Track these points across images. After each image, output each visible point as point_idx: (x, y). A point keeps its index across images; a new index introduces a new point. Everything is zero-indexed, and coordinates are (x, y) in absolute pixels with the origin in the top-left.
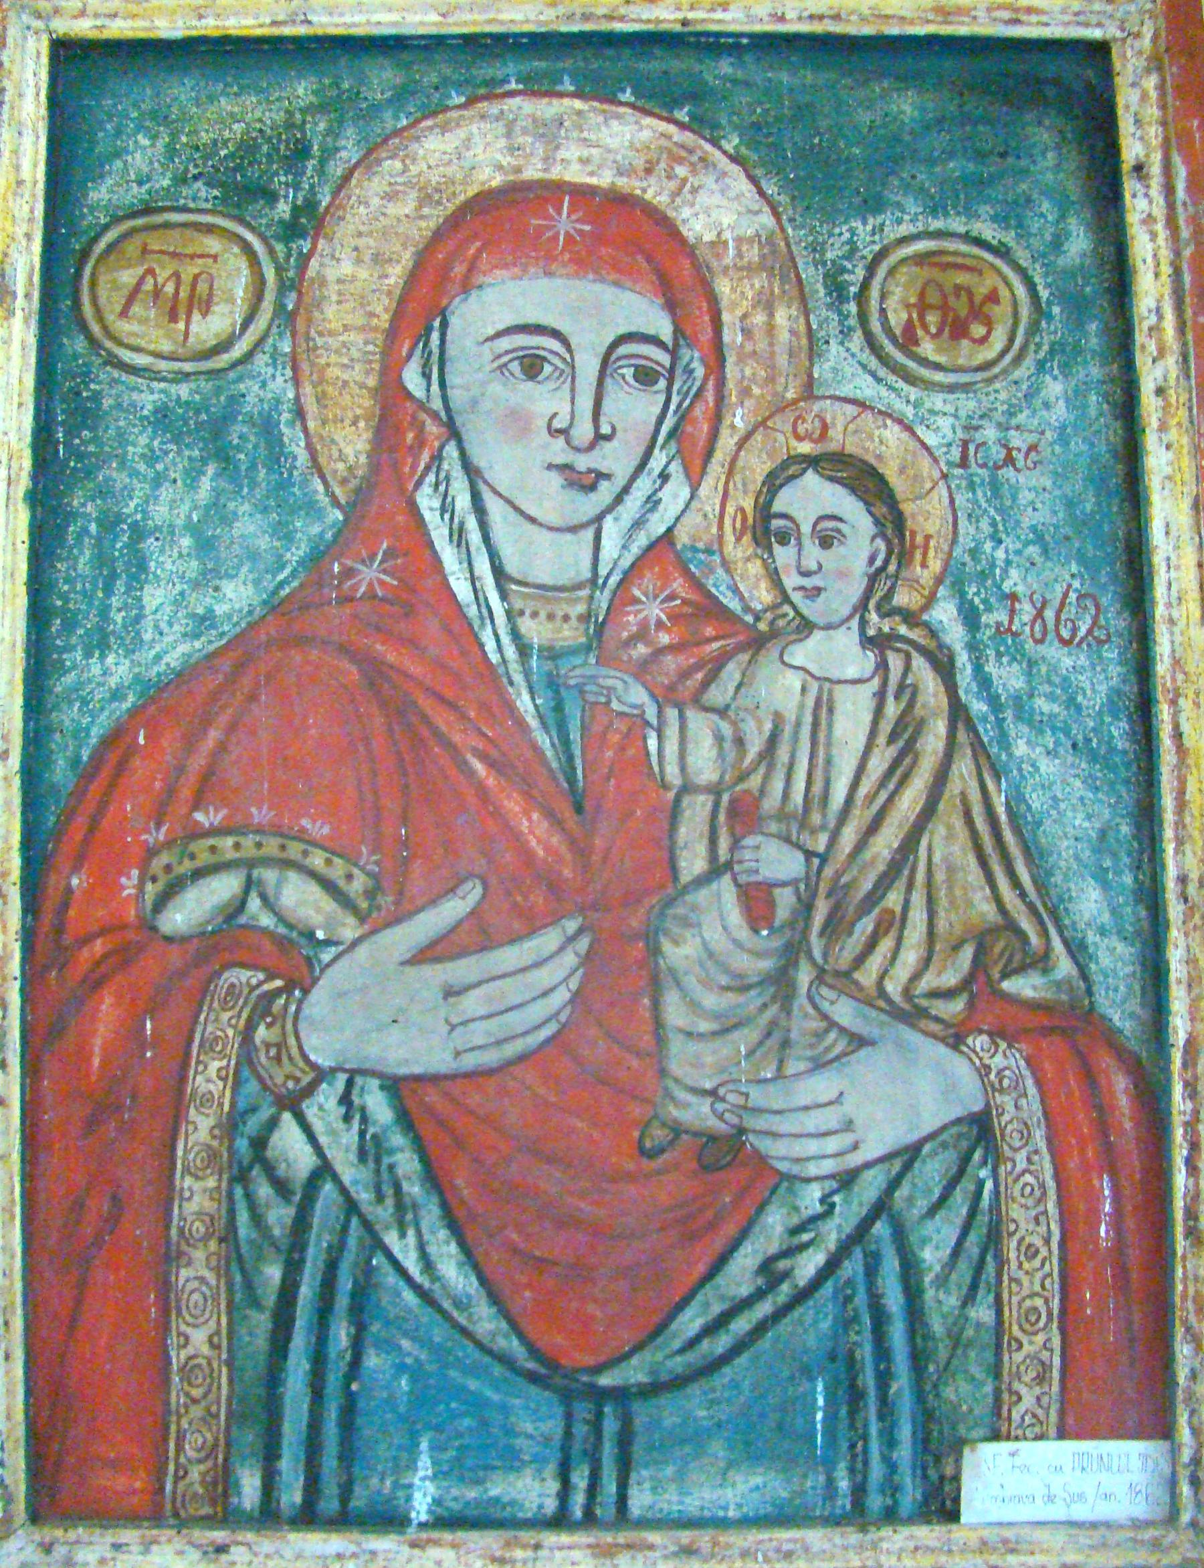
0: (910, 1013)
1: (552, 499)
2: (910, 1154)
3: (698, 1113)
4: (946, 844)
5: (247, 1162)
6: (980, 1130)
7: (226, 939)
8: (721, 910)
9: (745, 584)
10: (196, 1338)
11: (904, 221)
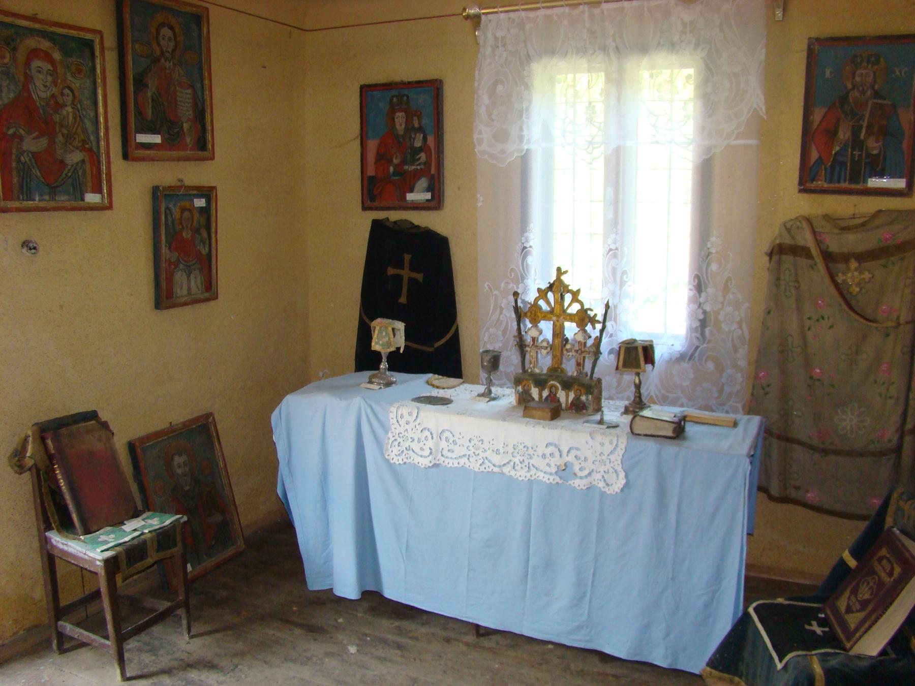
0: (77, 148)
1: (42, 88)
2: (77, 163)
3: (59, 158)
4: (79, 131)
5: (19, 161)
6: (83, 161)
7: (14, 135)
8: (60, 135)
9: (60, 100)
10: (15, 180)
11: (74, 59)
